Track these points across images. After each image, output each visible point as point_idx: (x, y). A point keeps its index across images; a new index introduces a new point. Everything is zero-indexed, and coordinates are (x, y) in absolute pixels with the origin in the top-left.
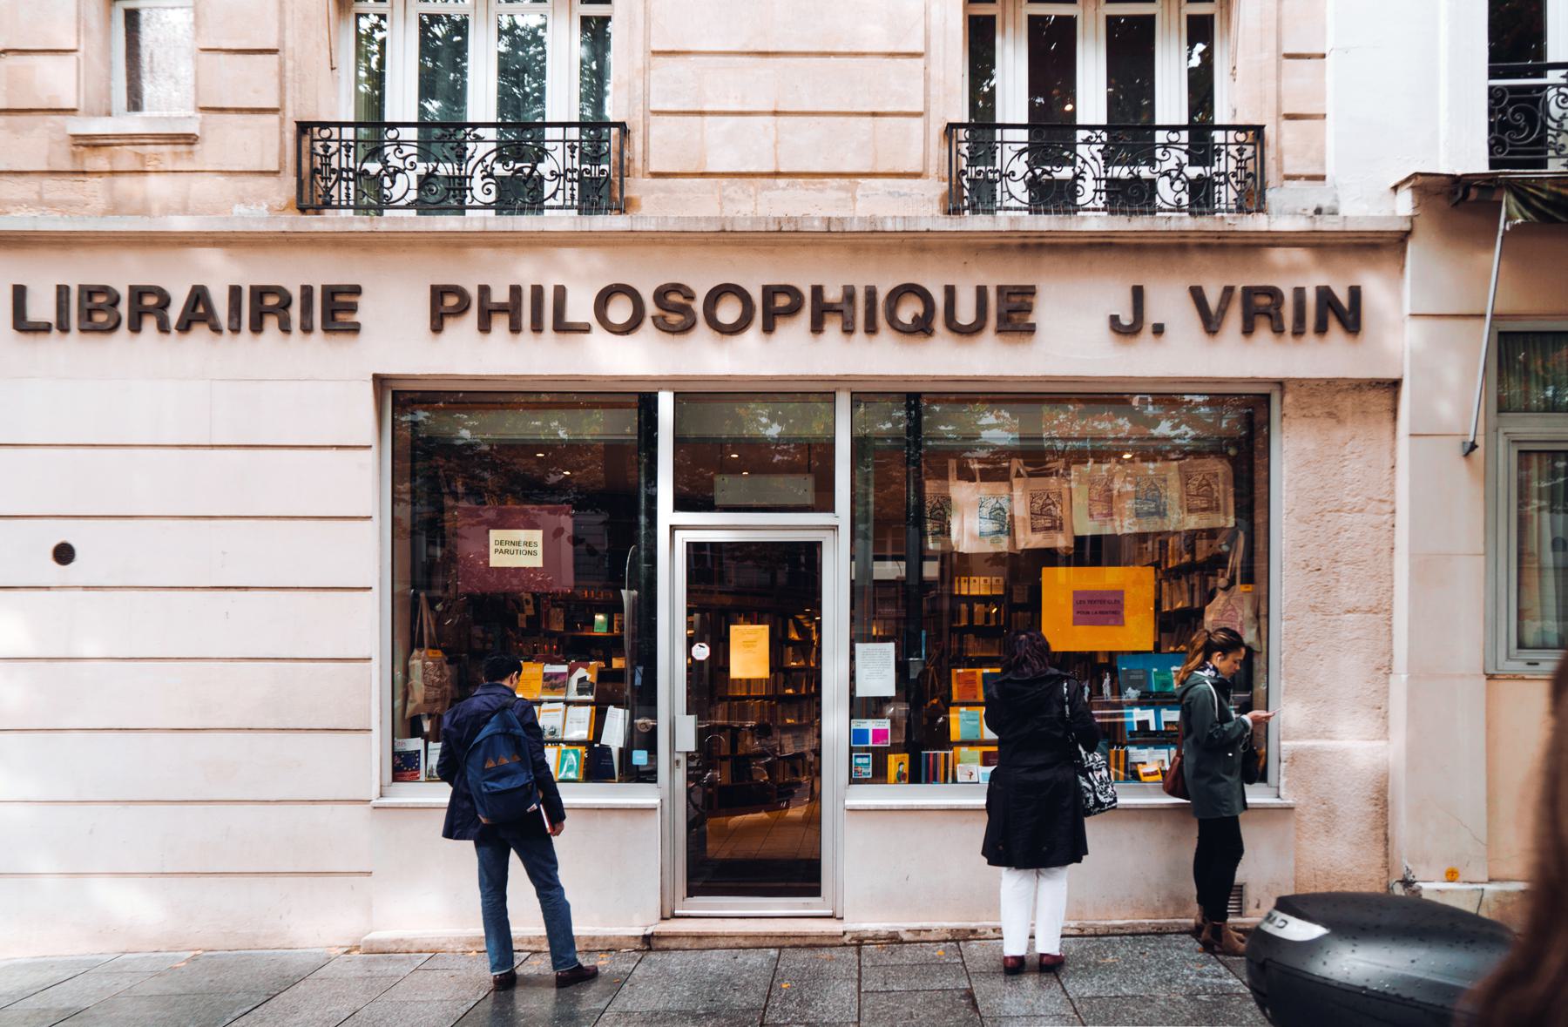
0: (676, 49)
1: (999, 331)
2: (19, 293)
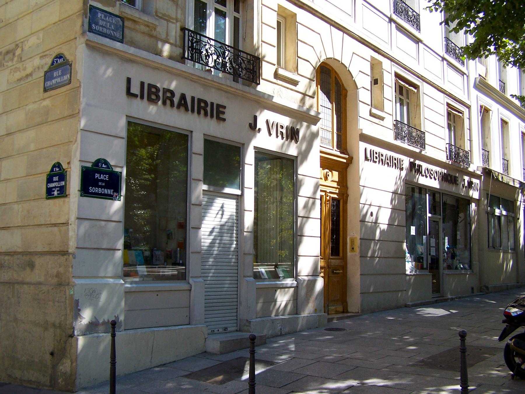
0: (263, 34)
1: (217, 118)
2: (129, 80)
